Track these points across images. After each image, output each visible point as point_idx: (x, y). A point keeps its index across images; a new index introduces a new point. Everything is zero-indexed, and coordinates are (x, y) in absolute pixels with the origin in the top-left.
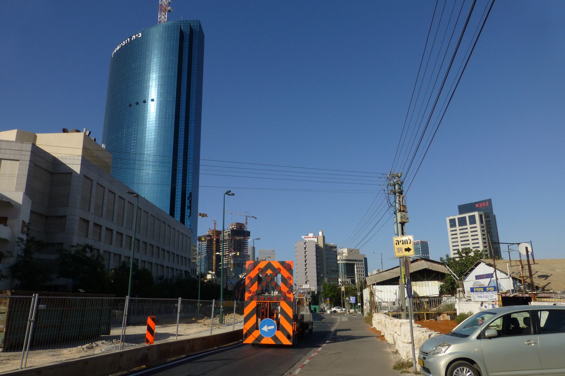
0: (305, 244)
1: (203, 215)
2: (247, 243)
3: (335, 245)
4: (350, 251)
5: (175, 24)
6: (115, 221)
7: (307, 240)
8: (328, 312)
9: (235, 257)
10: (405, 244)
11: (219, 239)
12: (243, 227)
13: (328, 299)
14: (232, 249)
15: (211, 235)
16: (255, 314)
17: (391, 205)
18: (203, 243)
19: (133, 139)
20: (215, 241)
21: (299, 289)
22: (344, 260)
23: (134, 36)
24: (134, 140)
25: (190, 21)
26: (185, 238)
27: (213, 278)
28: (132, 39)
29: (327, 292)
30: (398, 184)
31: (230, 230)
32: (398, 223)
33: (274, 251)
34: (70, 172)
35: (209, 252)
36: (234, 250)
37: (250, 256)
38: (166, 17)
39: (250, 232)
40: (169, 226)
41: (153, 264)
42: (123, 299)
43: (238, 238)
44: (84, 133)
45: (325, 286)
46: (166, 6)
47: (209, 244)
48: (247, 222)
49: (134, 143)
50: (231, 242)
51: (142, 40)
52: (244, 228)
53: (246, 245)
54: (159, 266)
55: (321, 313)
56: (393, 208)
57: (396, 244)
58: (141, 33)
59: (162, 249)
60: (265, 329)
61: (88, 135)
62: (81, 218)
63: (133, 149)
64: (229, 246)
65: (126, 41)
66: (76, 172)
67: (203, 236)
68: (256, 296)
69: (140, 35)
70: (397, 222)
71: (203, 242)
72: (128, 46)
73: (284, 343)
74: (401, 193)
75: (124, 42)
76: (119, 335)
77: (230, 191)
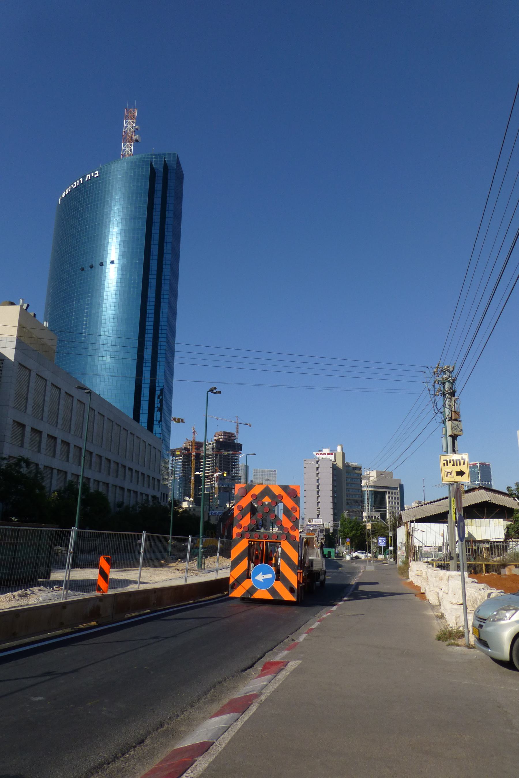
0: (318, 463)
1: (179, 420)
2: (237, 460)
3: (359, 466)
4: (380, 474)
5: (144, 158)
6: (59, 426)
7: (320, 458)
8: (348, 558)
9: (221, 478)
10: (457, 465)
11: (200, 454)
12: (232, 438)
13: (348, 540)
14: (217, 468)
15: (189, 447)
17: (439, 411)
20: (194, 456)
21: (307, 525)
22: (372, 487)
23: (89, 175)
24: (87, 316)
25: (165, 154)
26: (153, 450)
27: (191, 506)
28: (86, 180)
29: (346, 530)
30: (449, 381)
31: (215, 442)
32: (448, 436)
33: (275, 471)
35: (185, 470)
36: (220, 469)
38: (132, 148)
39: (242, 444)
41: (110, 486)
42: (68, 531)
43: (226, 453)
45: (345, 521)
46: (132, 134)
47: (186, 461)
49: (86, 320)
50: (216, 458)
51: (100, 180)
52: (233, 440)
53: (237, 462)
54: (118, 488)
55: (337, 558)
56: (441, 415)
57: (444, 465)
59: (122, 465)
60: (260, 577)
61: (25, 308)
62: (14, 421)
64: (212, 464)
65: (78, 181)
66: (9, 359)
67: (178, 449)
69: (96, 173)
70: (446, 434)
71: (178, 457)
72: (80, 188)
74: (453, 394)
75: (75, 183)
77: (215, 388)
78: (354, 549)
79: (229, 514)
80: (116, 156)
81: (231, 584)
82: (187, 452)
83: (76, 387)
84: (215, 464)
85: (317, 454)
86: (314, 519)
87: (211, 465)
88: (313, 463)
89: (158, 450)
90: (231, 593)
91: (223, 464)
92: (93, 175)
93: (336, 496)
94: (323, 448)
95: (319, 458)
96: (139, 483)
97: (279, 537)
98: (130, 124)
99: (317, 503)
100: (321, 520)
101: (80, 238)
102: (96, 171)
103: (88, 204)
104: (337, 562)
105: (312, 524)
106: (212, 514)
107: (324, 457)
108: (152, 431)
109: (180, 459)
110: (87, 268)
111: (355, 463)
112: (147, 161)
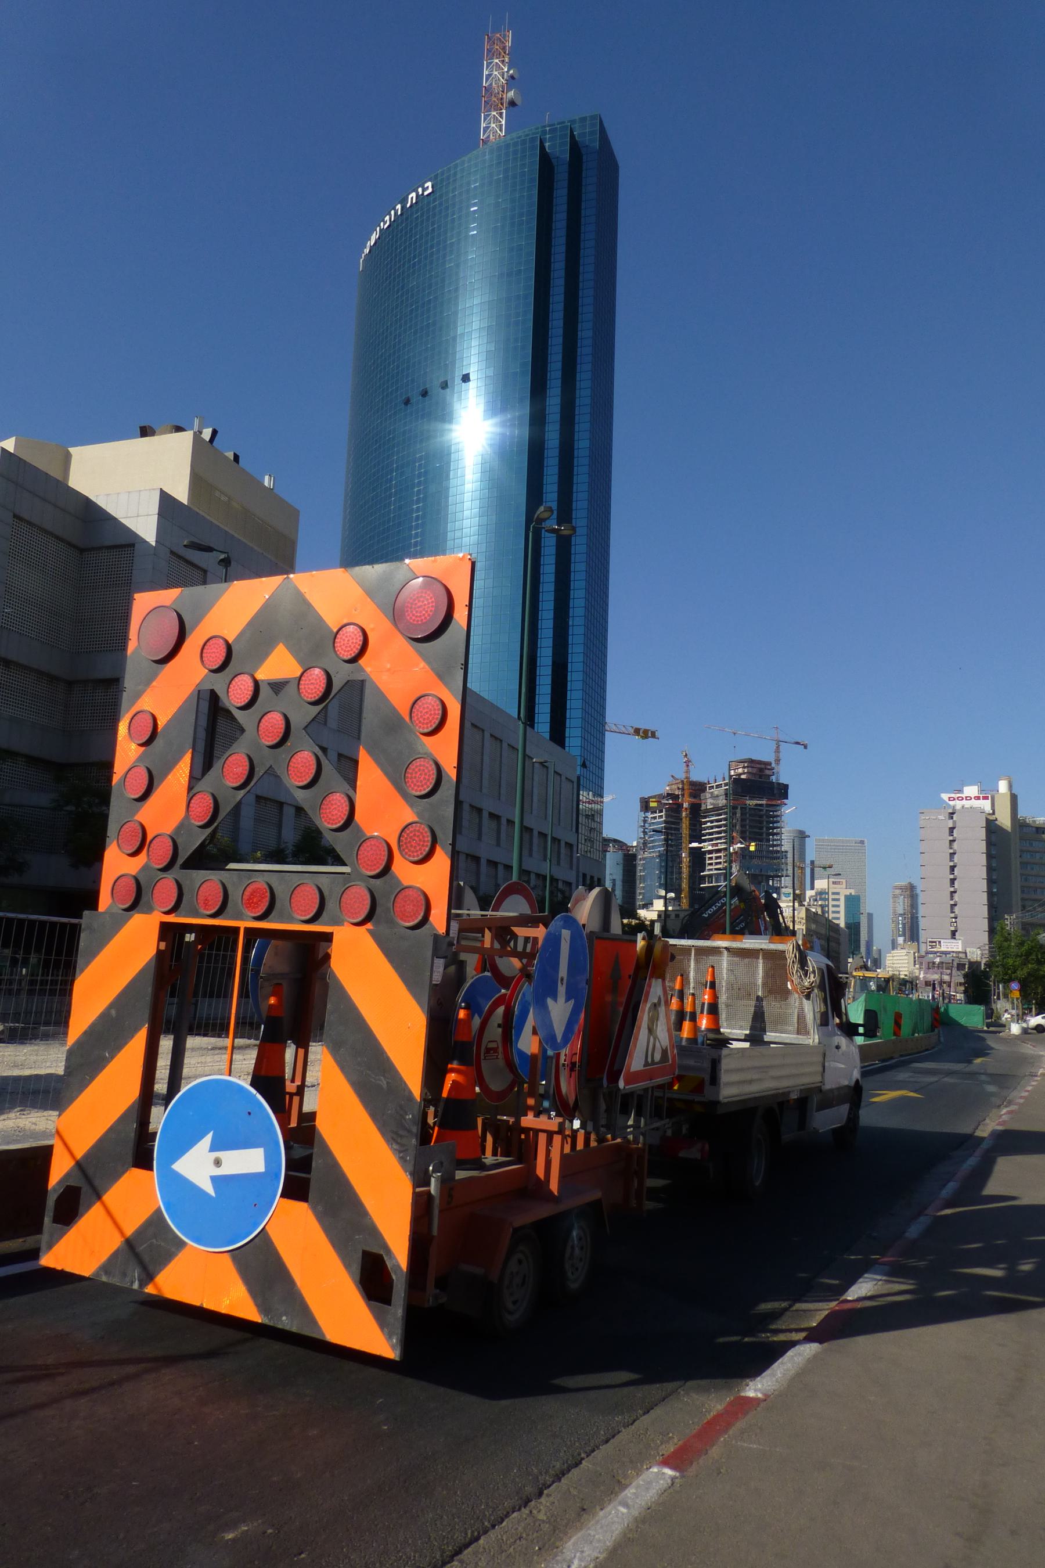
0: (952, 818)
1: (646, 732)
2: (779, 819)
7: (958, 807)
8: (1015, 1029)
9: (744, 853)
11: (700, 805)
12: (767, 772)
13: (1015, 986)
14: (734, 834)
16: (137, 1030)
18: (655, 815)
19: (415, 498)
20: (686, 809)
21: (927, 953)
23: (414, 195)
24: (418, 501)
25: (573, 122)
27: (670, 908)
28: (408, 205)
29: (1010, 961)
33: (862, 842)
34: (129, 542)
38: (503, 122)
39: (788, 785)
40: (496, 738)
43: (752, 803)
44: (195, 433)
45: (1006, 940)
46: (503, 92)
47: (672, 820)
49: (418, 509)
50: (735, 814)
51: (435, 200)
54: (462, 858)
55: (991, 1029)
61: (208, 440)
63: (417, 527)
65: (393, 212)
68: (169, 878)
69: (428, 187)
73: (335, 1333)
75: (387, 218)
78: (1033, 1006)
79: (704, 915)
80: (470, 137)
81: (54, 1189)
82: (671, 802)
83: (185, 543)
85: (949, 798)
86: (942, 941)
87: (723, 828)
88: (941, 817)
89: (567, 778)
90: (50, 1247)
91: (748, 827)
92: (420, 193)
93: (995, 890)
94: (964, 785)
95: (954, 807)
96: (535, 854)
97: (331, 905)
98: (498, 68)
99: (952, 905)
100: (960, 942)
101: (400, 335)
102: (426, 182)
103: (415, 257)
104: (983, 1039)
105: (938, 952)
108: (562, 744)
110: (416, 398)
111: (1042, 819)
112: (533, 140)
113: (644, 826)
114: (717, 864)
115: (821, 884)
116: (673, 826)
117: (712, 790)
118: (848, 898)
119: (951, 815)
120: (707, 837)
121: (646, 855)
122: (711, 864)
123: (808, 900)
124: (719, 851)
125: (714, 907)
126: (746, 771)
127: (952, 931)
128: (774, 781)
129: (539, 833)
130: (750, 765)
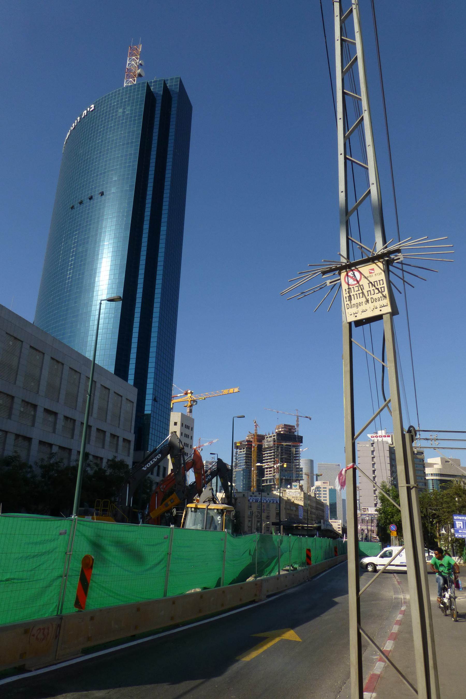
0: (373, 446)
4: (445, 462)
7: (376, 440)
18: (241, 450)
19: (71, 255)
22: (437, 475)
24: (72, 256)
28: (83, 117)
33: (339, 465)
37: (303, 470)
43: (284, 444)
48: (298, 423)
50: (278, 450)
51: (95, 113)
52: (294, 432)
58: (94, 104)
64: (274, 455)
65: (76, 121)
75: (74, 125)
76: (403, 535)
79: (144, 468)
84: (277, 456)
85: (371, 436)
86: (369, 508)
88: (368, 446)
89: (127, 399)
92: (88, 110)
99: (374, 490)
105: (367, 514)
106: (253, 501)
107: (380, 439)
109: (243, 451)
113: (236, 456)
114: (270, 474)
115: (317, 484)
116: (249, 456)
117: (268, 439)
118: (331, 490)
119: (372, 444)
120: (265, 461)
121: (237, 469)
122: (267, 474)
123: (312, 491)
124: (271, 468)
125: (151, 462)
126: (283, 430)
127: (375, 504)
128: (296, 434)
129: (111, 434)
130: (285, 427)
